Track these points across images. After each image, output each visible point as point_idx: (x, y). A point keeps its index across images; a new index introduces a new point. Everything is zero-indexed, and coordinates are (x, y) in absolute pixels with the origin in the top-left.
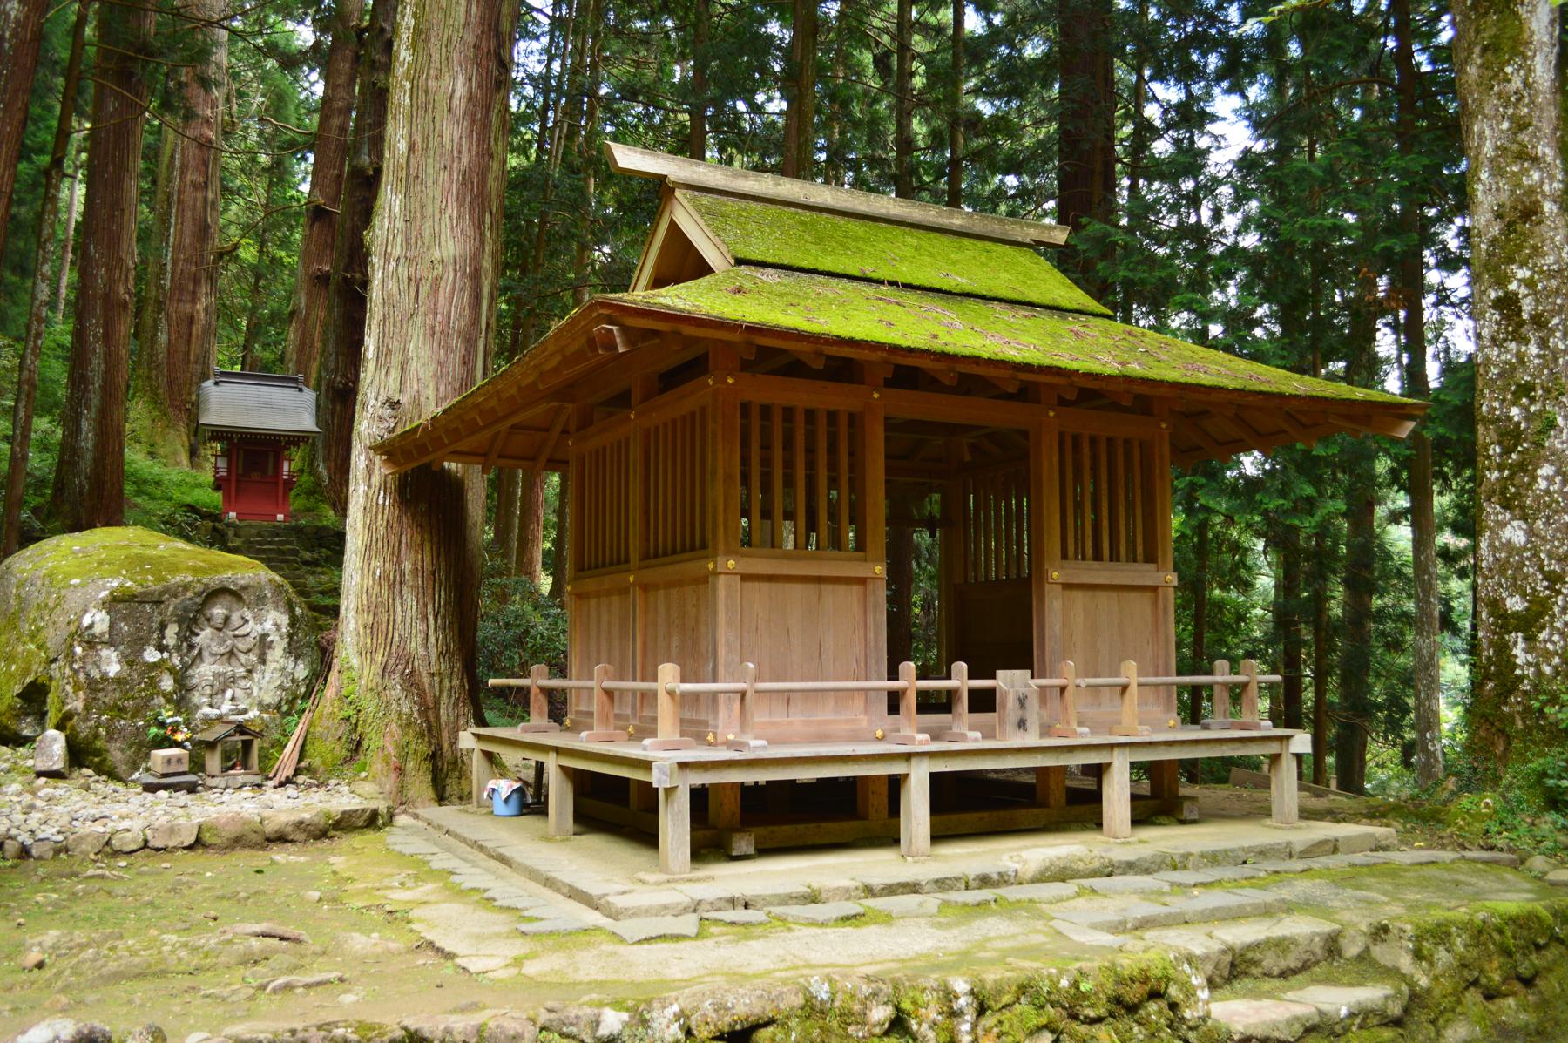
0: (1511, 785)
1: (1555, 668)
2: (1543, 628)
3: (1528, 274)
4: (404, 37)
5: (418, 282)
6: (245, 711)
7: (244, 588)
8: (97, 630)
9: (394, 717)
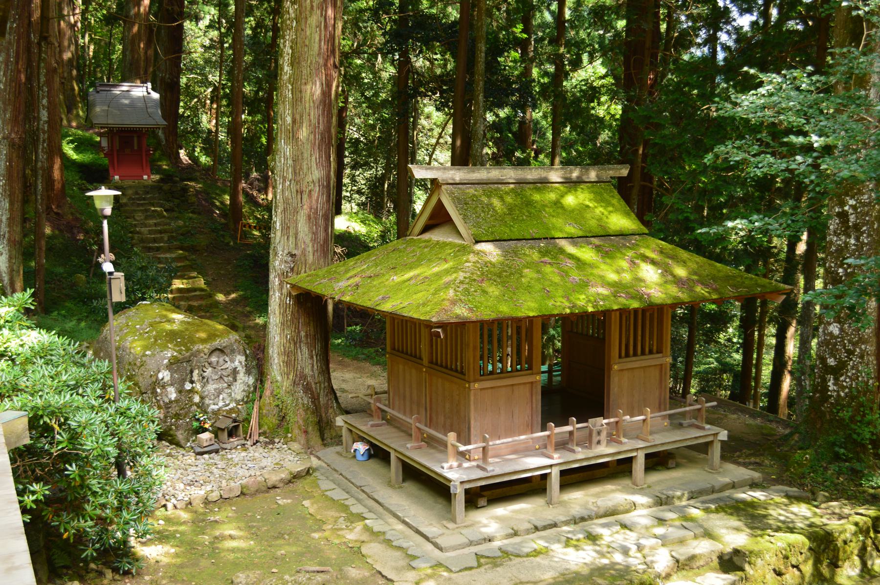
0: (821, 445)
1: (846, 394)
2: (842, 375)
3: (854, 203)
4: (286, 58)
5: (301, 193)
6: (229, 404)
7: (225, 347)
8: (166, 380)
9: (301, 406)
